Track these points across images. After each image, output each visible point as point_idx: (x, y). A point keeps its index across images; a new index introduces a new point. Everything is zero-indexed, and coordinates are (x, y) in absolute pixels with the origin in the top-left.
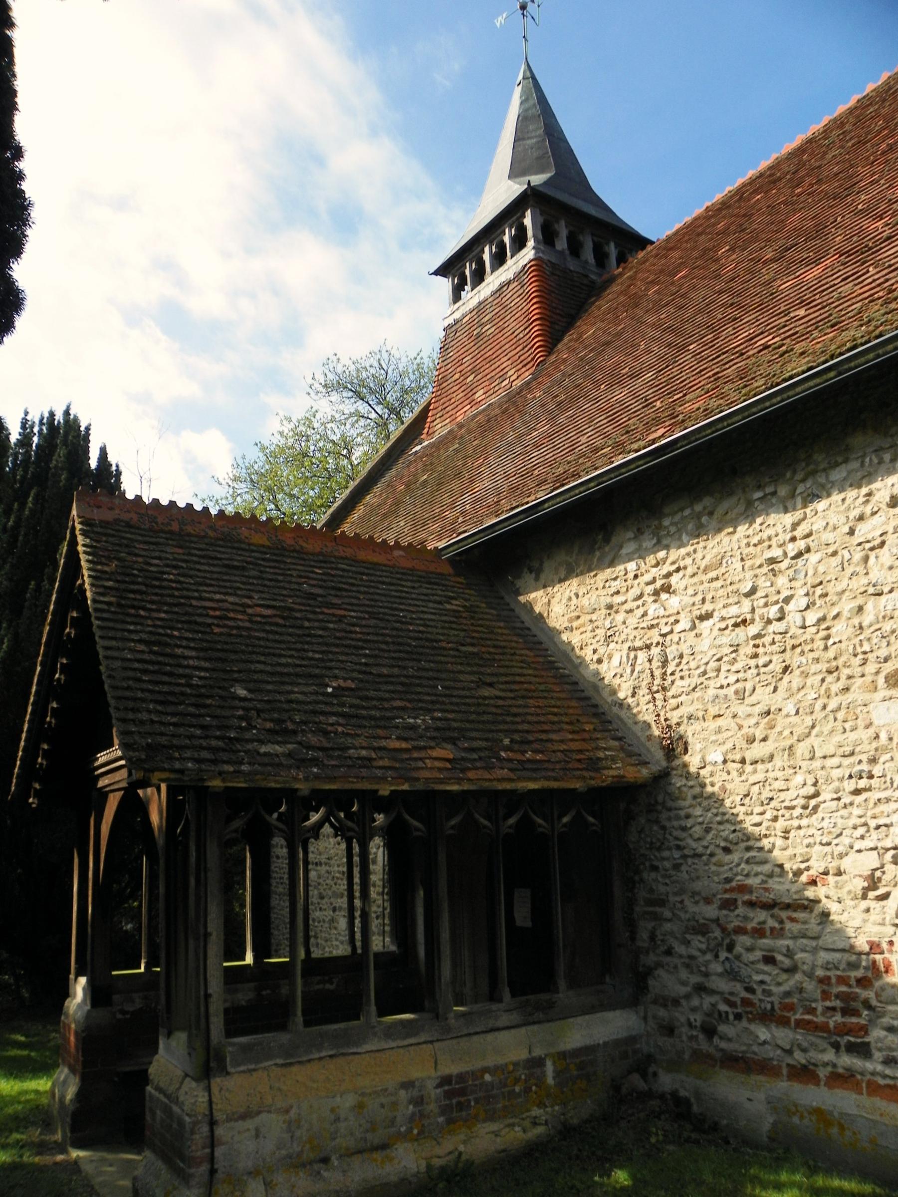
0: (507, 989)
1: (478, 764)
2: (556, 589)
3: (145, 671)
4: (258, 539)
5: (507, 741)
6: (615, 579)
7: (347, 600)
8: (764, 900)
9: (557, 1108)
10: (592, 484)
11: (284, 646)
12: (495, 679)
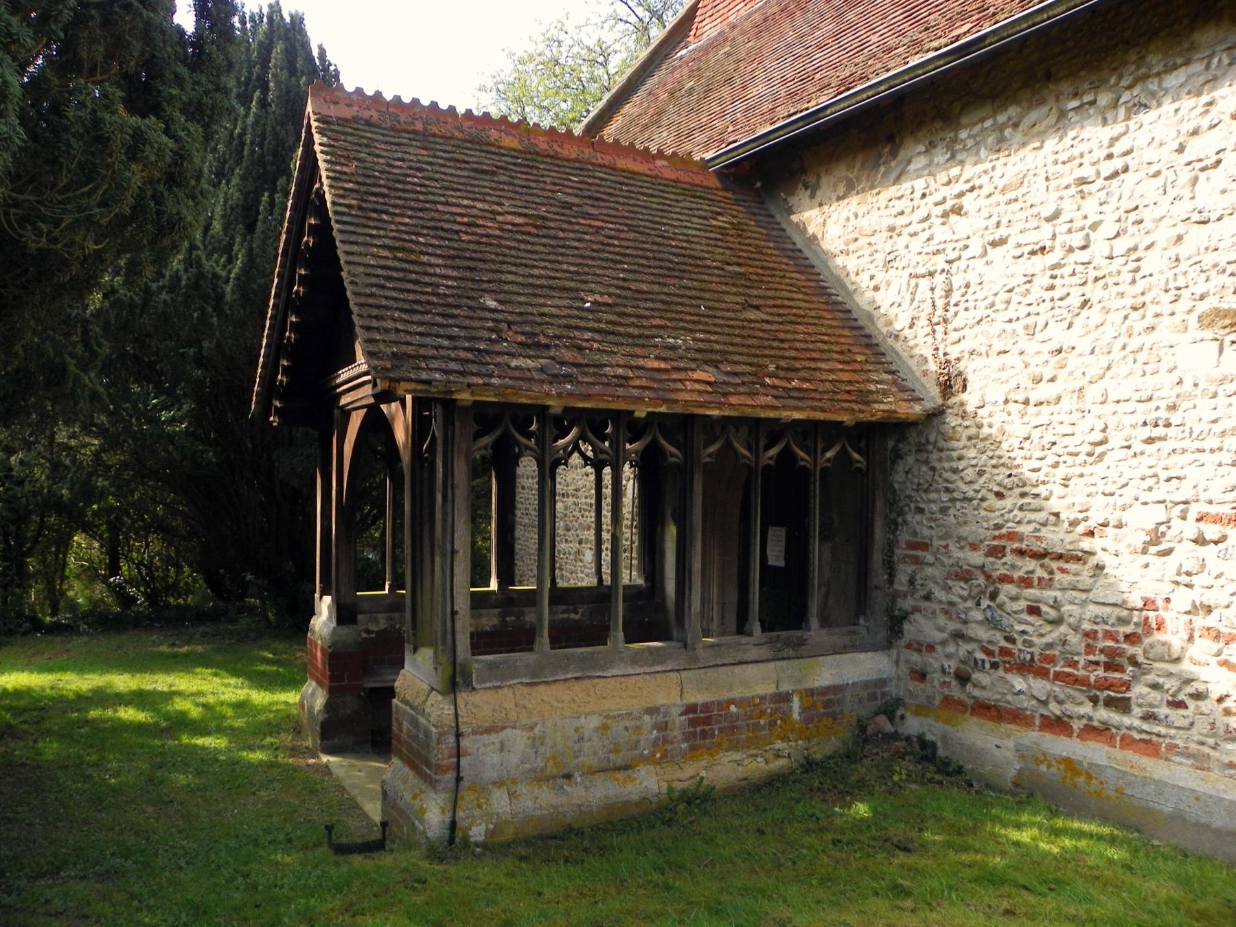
0: (758, 624)
1: (742, 389)
2: (833, 208)
3: (389, 278)
4: (509, 142)
5: (772, 368)
6: (900, 198)
7: (604, 211)
8: (1035, 549)
9: (800, 742)
10: (883, 88)
11: (536, 257)
12: (762, 302)
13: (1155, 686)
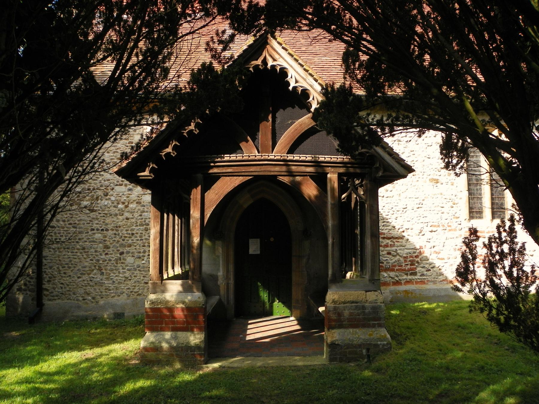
13: (423, 267)
